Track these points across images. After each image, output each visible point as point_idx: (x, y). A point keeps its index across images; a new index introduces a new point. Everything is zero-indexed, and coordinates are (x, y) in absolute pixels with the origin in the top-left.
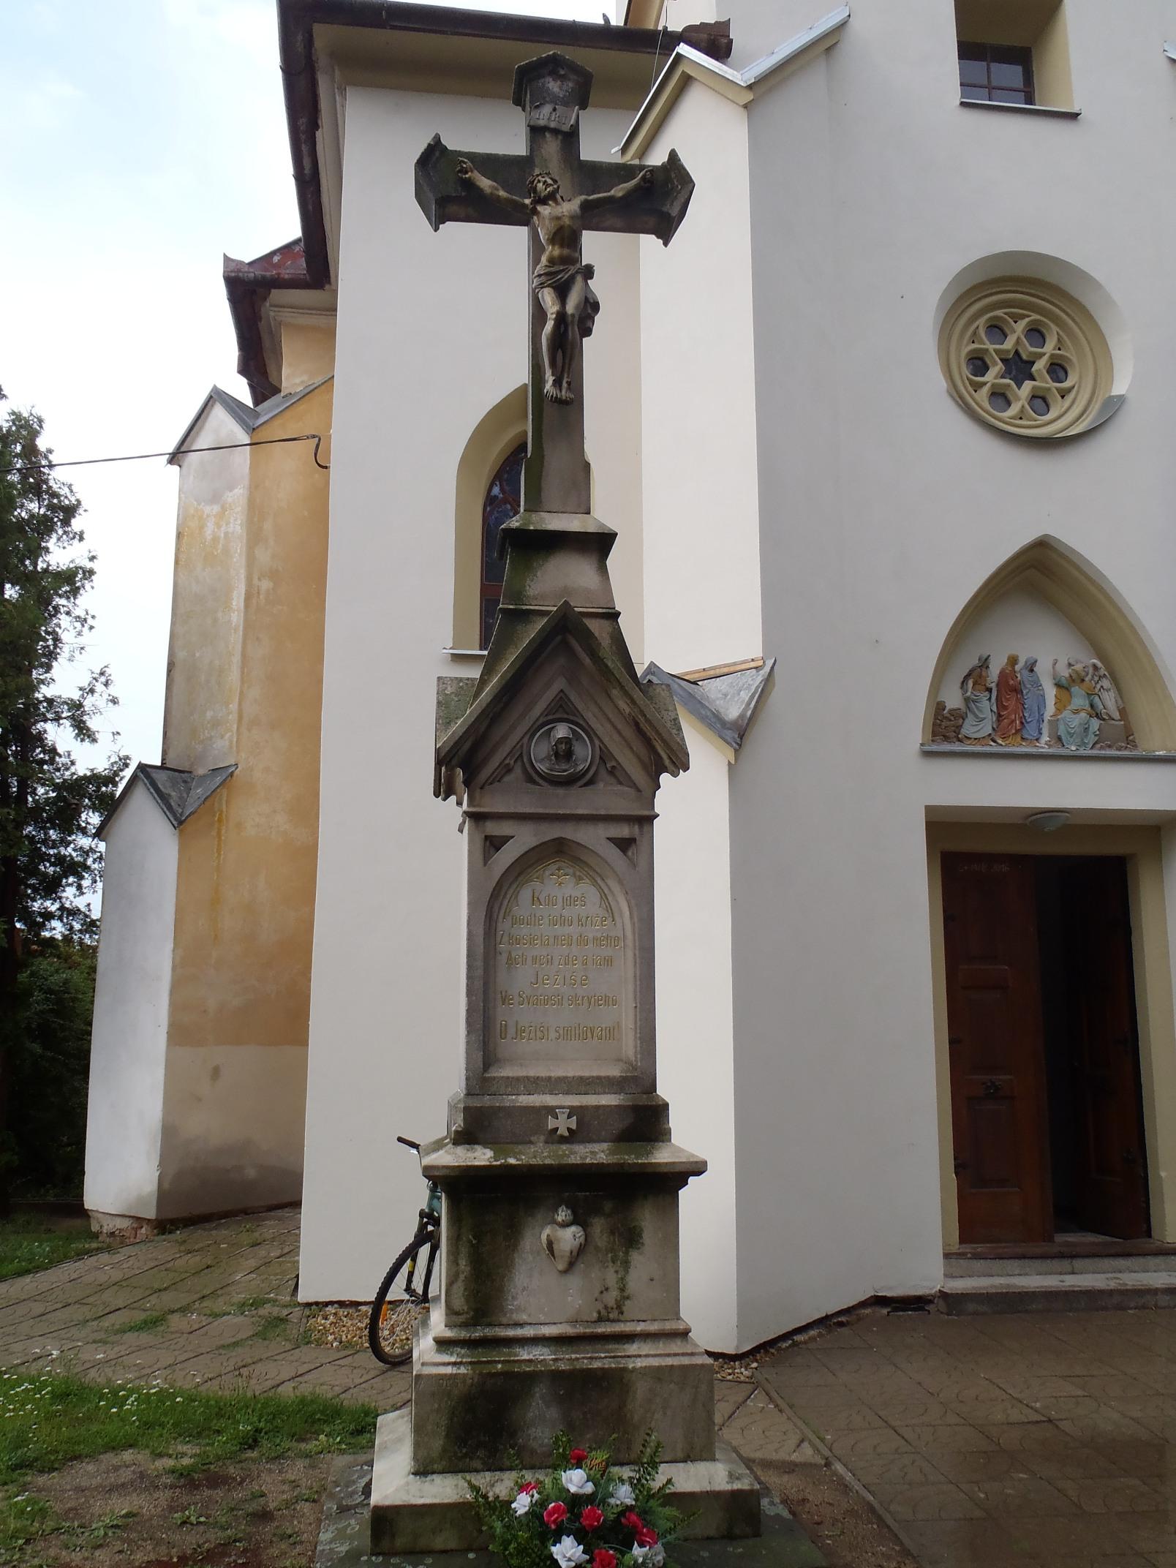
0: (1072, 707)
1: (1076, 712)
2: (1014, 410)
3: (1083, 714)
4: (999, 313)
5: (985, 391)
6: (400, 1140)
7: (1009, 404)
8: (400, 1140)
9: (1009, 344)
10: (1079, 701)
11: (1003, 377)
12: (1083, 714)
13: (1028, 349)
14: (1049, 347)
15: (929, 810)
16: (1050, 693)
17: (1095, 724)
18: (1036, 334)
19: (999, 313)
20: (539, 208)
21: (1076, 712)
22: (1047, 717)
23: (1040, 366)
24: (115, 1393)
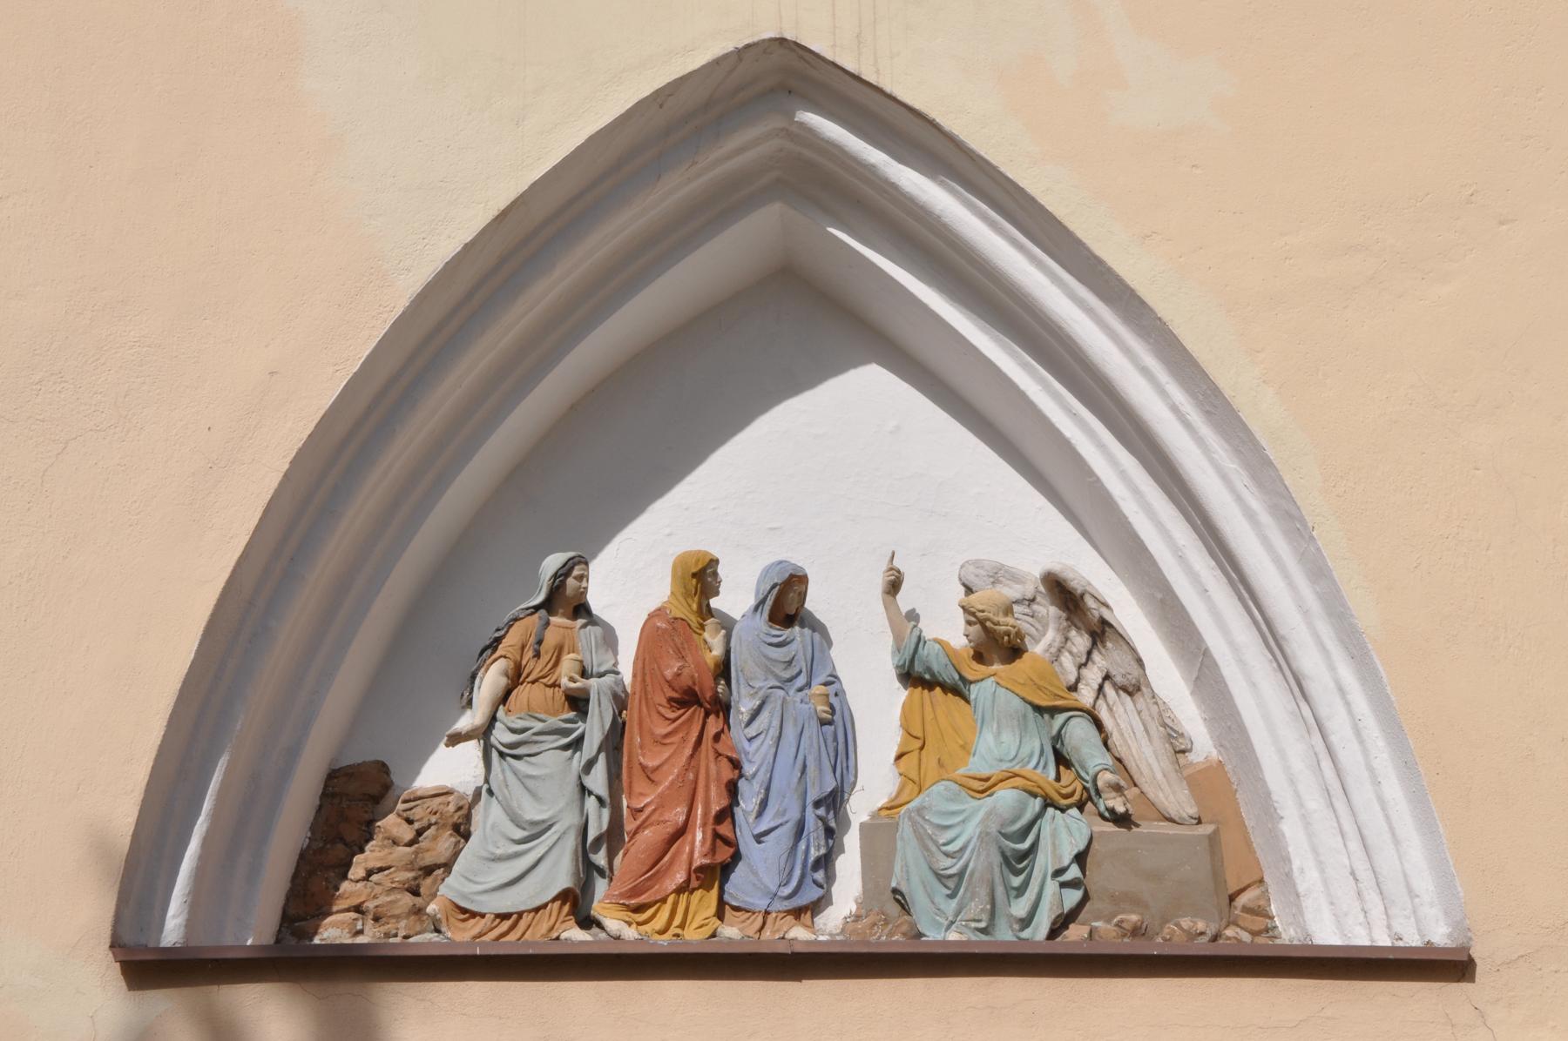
0: (978, 766)
1: (985, 787)
6: (1449, 967)
8: (1449, 967)
10: (998, 737)
16: (878, 708)
21: (985, 787)
22: (860, 807)
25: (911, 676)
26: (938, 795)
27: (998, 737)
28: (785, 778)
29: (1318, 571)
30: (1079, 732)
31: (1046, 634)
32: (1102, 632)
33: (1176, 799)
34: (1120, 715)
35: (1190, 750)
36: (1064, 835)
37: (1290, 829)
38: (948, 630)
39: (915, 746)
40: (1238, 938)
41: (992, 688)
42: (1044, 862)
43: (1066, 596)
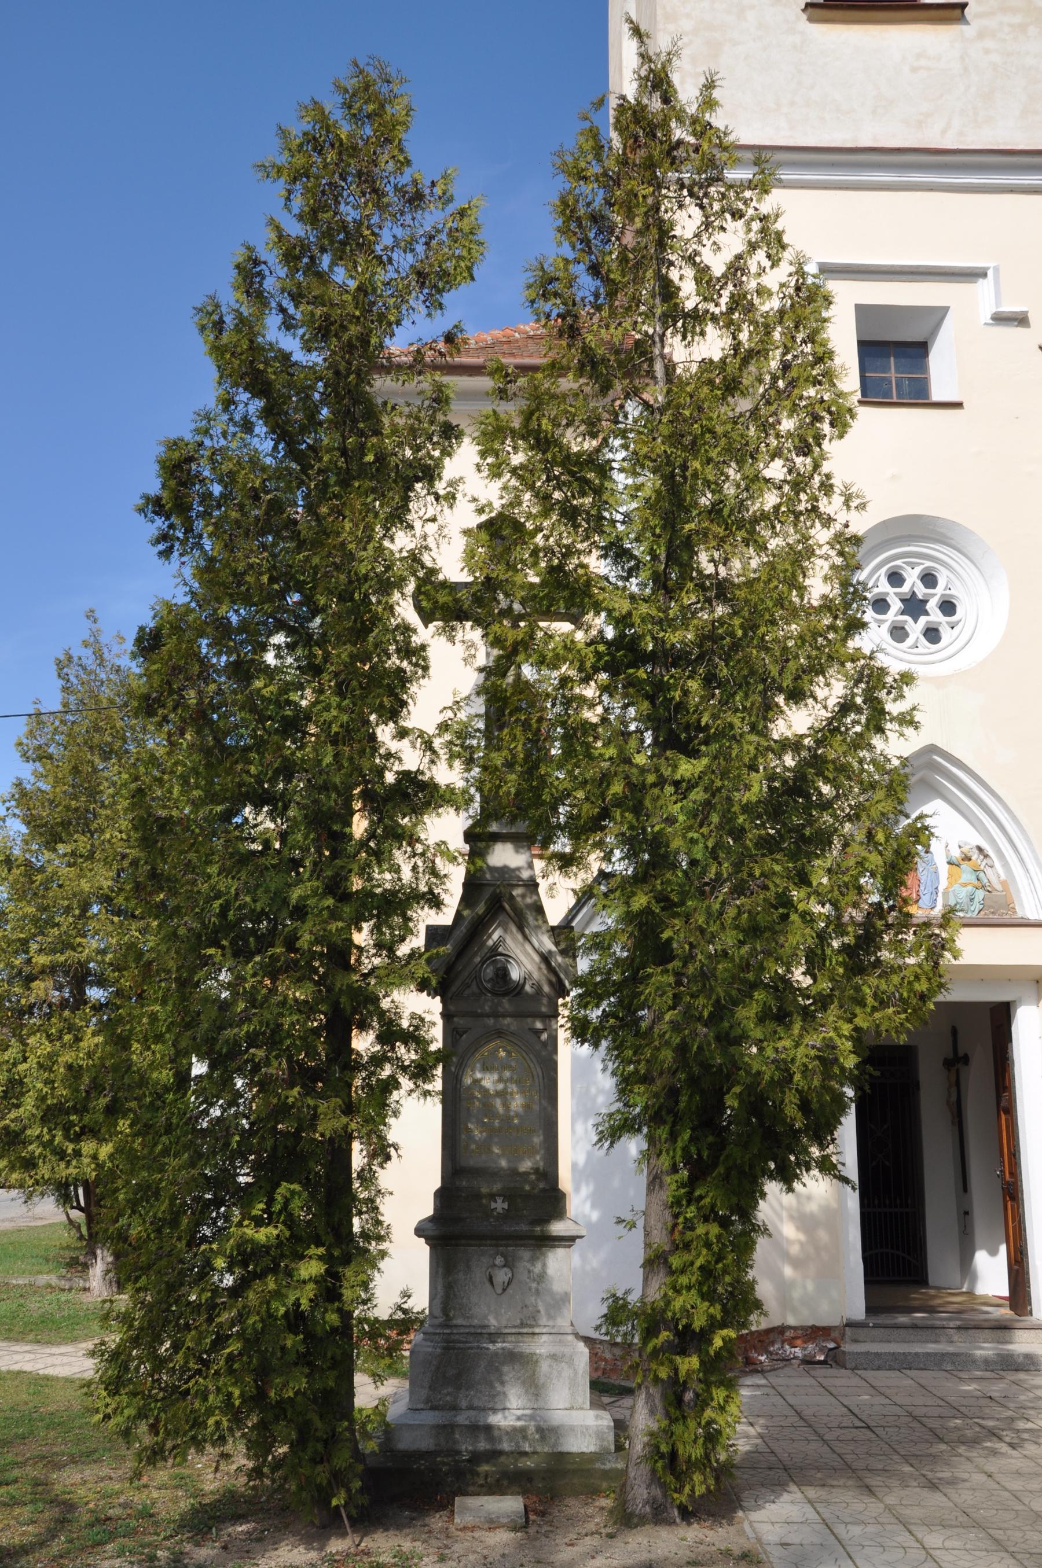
0: (962, 881)
1: (965, 885)
2: (910, 641)
3: (970, 888)
4: (899, 562)
5: (886, 627)
6: (958, 405)
7: (907, 635)
8: (958, 405)
9: (906, 588)
10: (966, 875)
11: (902, 613)
12: (970, 888)
13: (921, 591)
14: (940, 590)
15: (916, 1047)
16: (943, 869)
17: (980, 894)
18: (929, 579)
19: (899, 562)
20: (603, 614)
21: (965, 885)
22: (941, 889)
23: (932, 605)
24: (75, 1462)
25: (949, 863)
26: (956, 887)
27: (966, 875)
28: (929, 884)
29: (1033, 851)
30: (982, 875)
31: (975, 856)
32: (986, 856)
33: (999, 887)
34: (988, 871)
35: (147, 498)
36: (980, 894)
37: (1023, 895)
38: (956, 854)
39: (950, 875)
40: (1006, 918)
41: (965, 866)
42: (976, 900)
43: (980, 849)
